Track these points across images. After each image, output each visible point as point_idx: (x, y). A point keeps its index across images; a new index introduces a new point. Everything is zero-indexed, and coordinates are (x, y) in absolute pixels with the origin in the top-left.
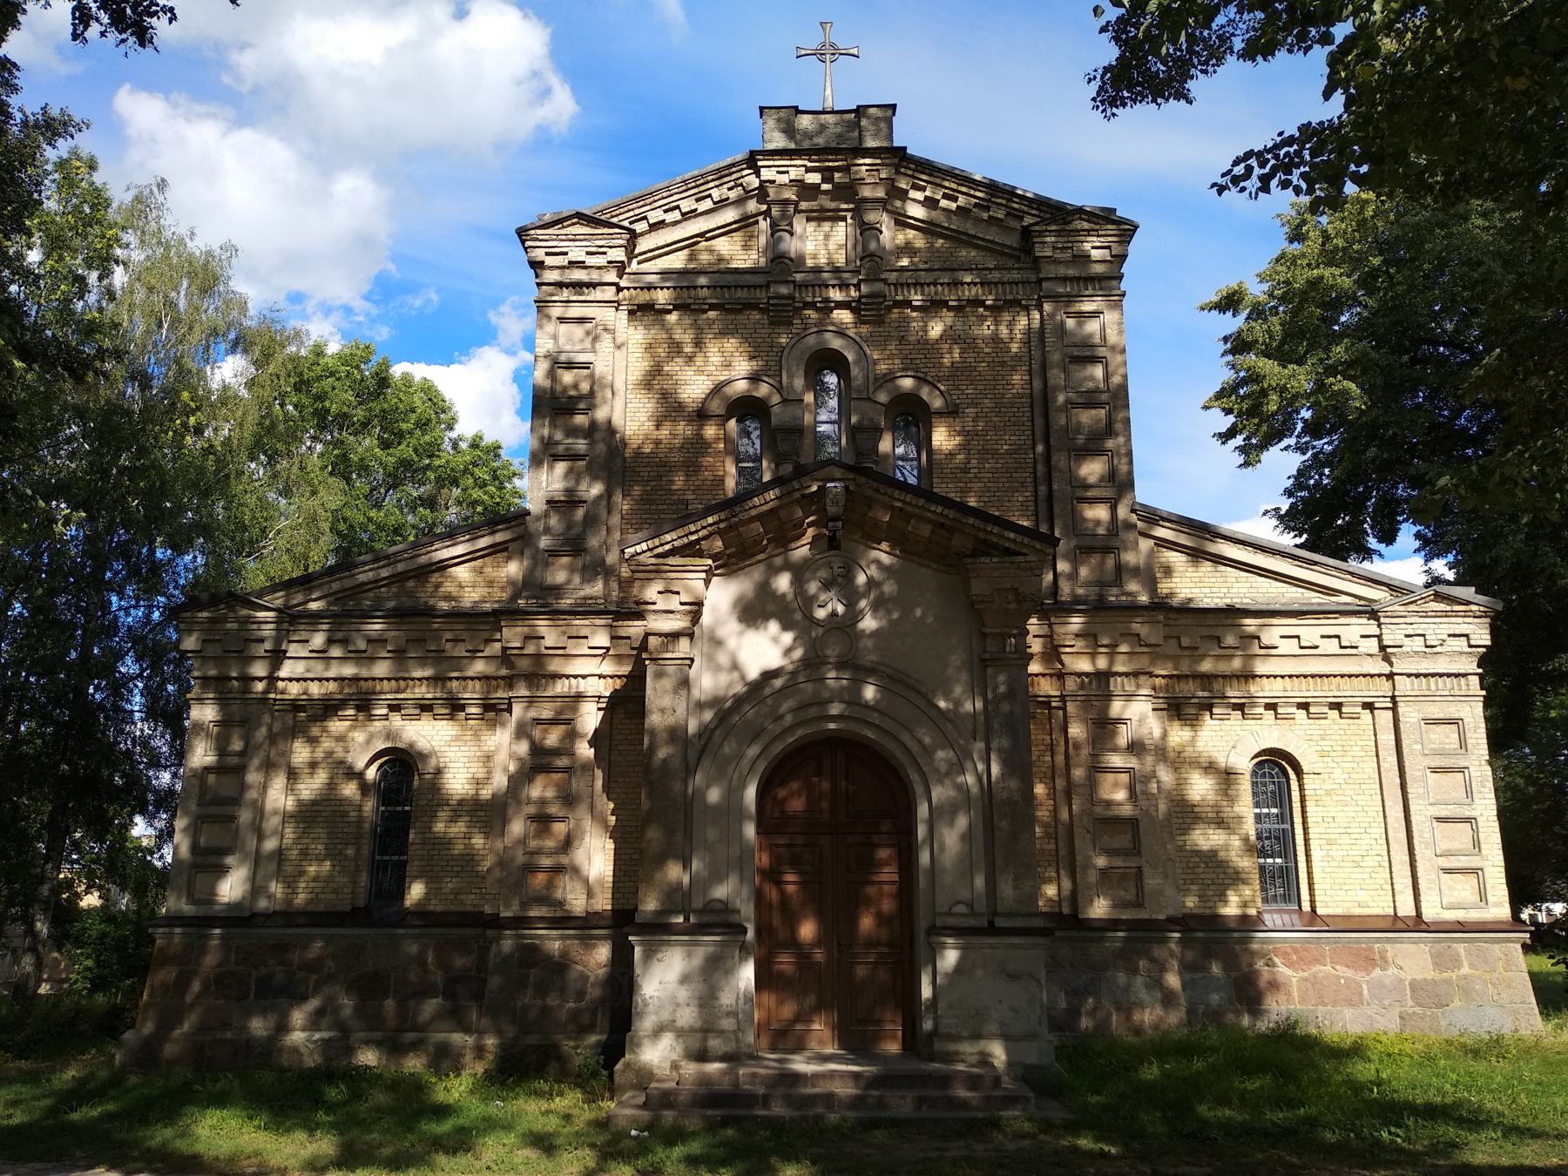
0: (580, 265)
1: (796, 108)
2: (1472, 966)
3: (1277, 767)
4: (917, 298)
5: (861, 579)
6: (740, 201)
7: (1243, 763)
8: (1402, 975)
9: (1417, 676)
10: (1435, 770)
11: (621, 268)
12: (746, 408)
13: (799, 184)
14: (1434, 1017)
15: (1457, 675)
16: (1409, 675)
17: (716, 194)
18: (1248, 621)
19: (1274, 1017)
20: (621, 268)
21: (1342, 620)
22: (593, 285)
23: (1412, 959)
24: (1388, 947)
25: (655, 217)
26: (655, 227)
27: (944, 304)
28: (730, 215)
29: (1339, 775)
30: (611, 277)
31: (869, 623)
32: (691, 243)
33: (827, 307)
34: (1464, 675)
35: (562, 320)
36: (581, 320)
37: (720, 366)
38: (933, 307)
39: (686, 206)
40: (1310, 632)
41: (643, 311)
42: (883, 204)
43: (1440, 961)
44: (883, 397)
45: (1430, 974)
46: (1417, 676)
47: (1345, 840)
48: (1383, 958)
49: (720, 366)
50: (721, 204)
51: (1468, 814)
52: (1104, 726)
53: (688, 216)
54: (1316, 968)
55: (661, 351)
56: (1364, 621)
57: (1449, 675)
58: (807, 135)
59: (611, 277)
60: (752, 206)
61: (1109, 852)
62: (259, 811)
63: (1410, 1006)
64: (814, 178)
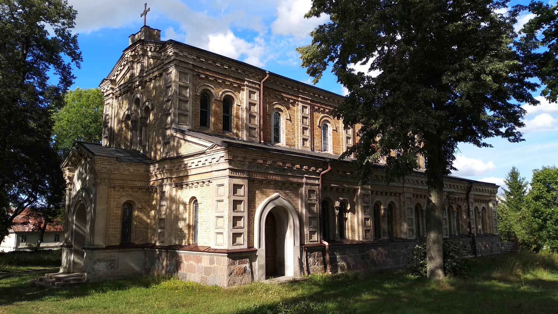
7: (187, 201)
11: (112, 89)
14: (207, 278)
17: (123, 64)
18: (185, 160)
19: (452, 279)
21: (201, 156)
22: (109, 94)
26: (117, 75)
28: (126, 68)
30: (111, 91)
31: (88, 178)
36: (108, 104)
43: (212, 262)
45: (208, 265)
46: (219, 170)
50: (124, 65)
53: (121, 70)
54: (190, 261)
59: (111, 91)
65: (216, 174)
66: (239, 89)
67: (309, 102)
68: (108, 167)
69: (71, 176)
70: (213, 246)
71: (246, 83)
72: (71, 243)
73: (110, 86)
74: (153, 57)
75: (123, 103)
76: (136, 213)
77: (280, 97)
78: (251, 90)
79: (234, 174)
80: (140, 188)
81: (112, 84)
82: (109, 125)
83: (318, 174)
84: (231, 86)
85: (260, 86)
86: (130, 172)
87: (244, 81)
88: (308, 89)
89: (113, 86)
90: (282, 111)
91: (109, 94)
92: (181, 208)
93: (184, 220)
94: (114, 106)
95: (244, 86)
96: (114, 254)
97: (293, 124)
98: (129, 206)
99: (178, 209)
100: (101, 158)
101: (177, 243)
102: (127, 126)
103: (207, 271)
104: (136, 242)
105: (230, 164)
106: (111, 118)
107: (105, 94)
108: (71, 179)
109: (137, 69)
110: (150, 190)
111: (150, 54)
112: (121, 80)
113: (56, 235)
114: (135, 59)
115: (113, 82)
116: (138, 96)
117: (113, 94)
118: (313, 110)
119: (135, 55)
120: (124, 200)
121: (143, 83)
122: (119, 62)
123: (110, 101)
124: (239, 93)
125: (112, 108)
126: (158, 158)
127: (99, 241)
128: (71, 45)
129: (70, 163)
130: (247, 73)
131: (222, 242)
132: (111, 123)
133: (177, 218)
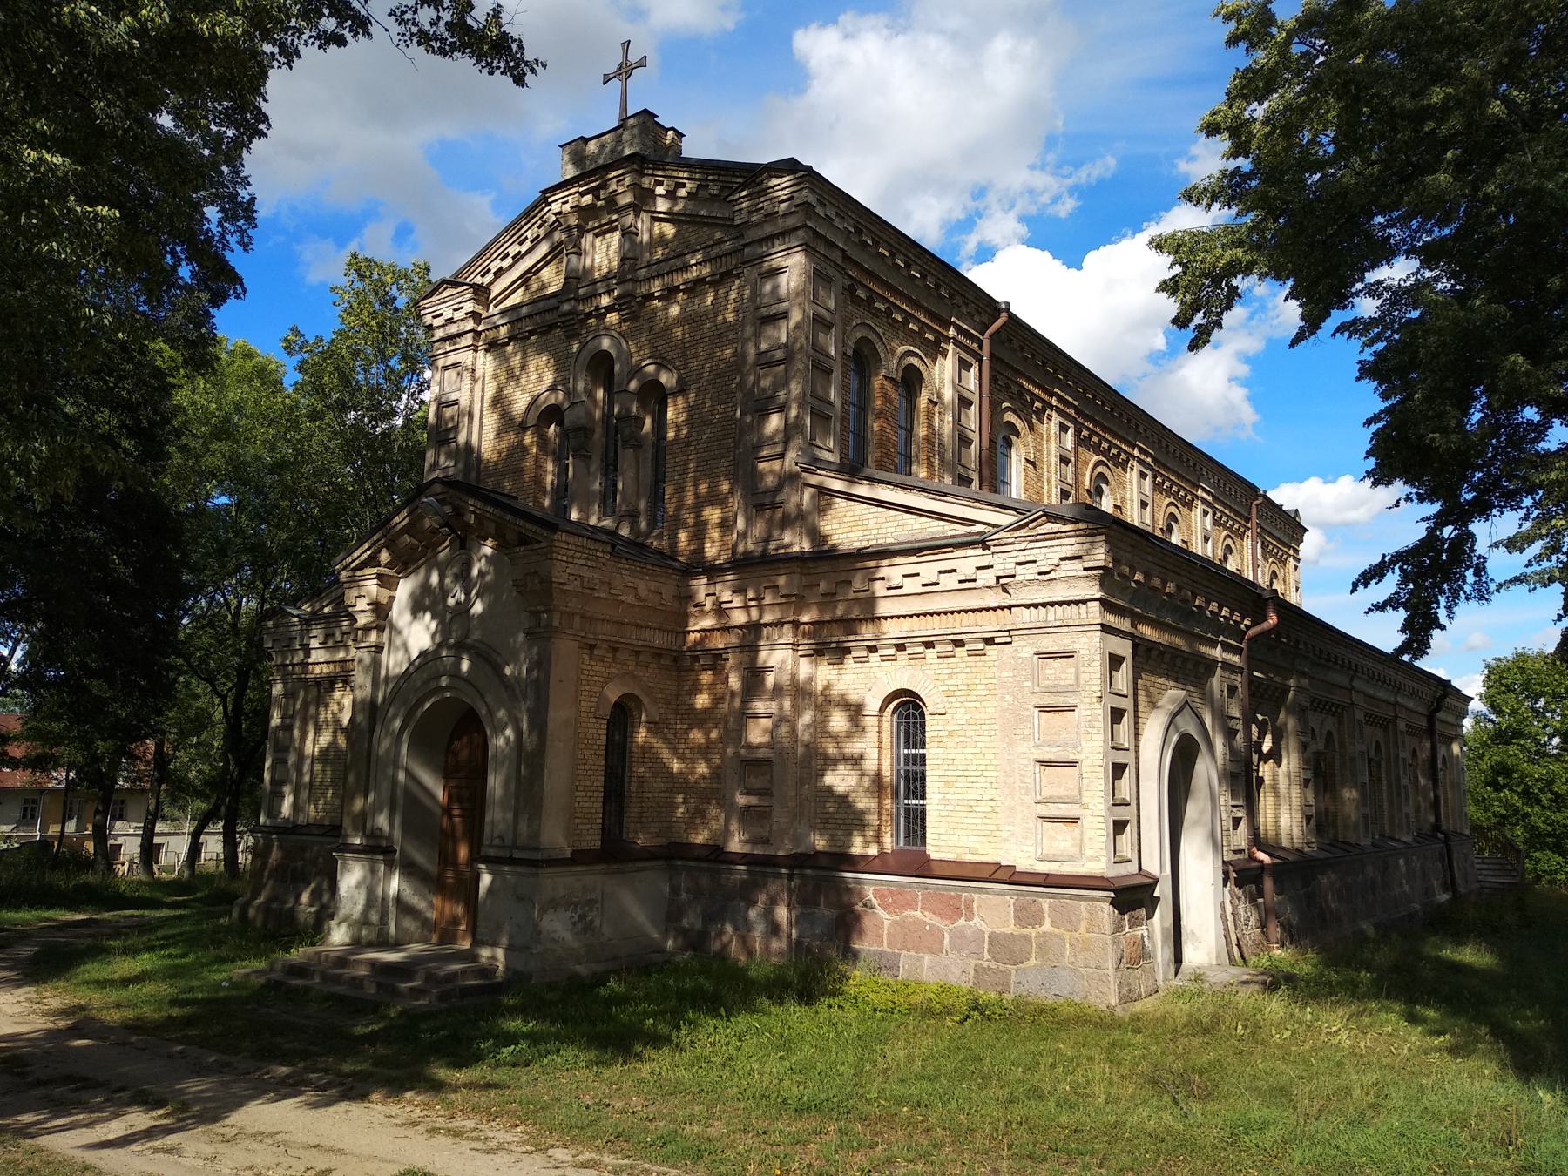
0: (450, 321)
1: (582, 138)
2: (1054, 924)
3: (908, 707)
4: (656, 287)
5: (475, 572)
6: (548, 235)
8: (984, 927)
9: (1036, 606)
10: (1044, 709)
11: (476, 316)
12: (552, 414)
13: (577, 208)
15: (1077, 603)
16: (1028, 606)
20: (476, 316)
21: (958, 553)
22: (461, 335)
23: (993, 911)
24: (976, 896)
25: (495, 266)
26: (499, 273)
27: (676, 289)
28: (544, 248)
29: (962, 716)
30: (470, 325)
31: (478, 608)
32: (525, 278)
33: (601, 314)
34: (1084, 602)
35: (445, 368)
36: (454, 366)
37: (537, 379)
38: (670, 293)
39: (513, 250)
40: (928, 569)
41: (493, 346)
42: (636, 208)
43: (1027, 916)
44: (633, 385)
45: (1011, 928)
46: (1036, 606)
47: (961, 783)
48: (969, 907)
49: (537, 379)
50: (536, 241)
51: (1071, 757)
52: (754, 676)
53: (518, 257)
55: (503, 379)
56: (979, 551)
57: (1068, 603)
58: (595, 157)
59: (470, 325)
60: (558, 236)
61: (749, 791)
62: (301, 757)
63: (986, 961)
64: (588, 199)
65: (1025, 617)
66: (935, 350)
67: (1072, 412)
68: (587, 574)
69: (384, 601)
70: (1025, 861)
71: (952, 332)
72: (390, 837)
73: (469, 306)
74: (671, 217)
75: (523, 366)
76: (642, 735)
77: (1015, 389)
78: (965, 356)
79: (1111, 620)
80: (658, 654)
81: (477, 301)
82: (462, 438)
83: (1240, 635)
84: (916, 338)
85: (980, 347)
86: (636, 596)
87: (947, 324)
88: (1075, 371)
89: (479, 309)
90: (1018, 435)
91: (461, 335)
92: (838, 721)
93: (856, 760)
94: (479, 373)
95: (947, 340)
96: (593, 880)
97: (1040, 479)
98: (621, 716)
99: (821, 726)
100: (572, 540)
101: (820, 843)
102: (542, 441)
103: (1006, 949)
104: (641, 841)
105: (1102, 586)
106: (471, 416)
107: (439, 334)
108: (381, 610)
109: (602, 254)
110: (684, 662)
111: (662, 206)
112: (510, 290)
113: (26, 801)
114: (590, 219)
115: (481, 293)
116: (606, 343)
117: (477, 334)
118: (1080, 441)
119: (592, 206)
120: (613, 694)
121: (632, 306)
122: (513, 229)
123: (466, 357)
124: (935, 361)
125: (474, 380)
126: (710, 550)
127: (554, 836)
128: (225, 168)
129: (384, 556)
130: (958, 300)
131: (1074, 851)
132: (470, 433)
133: (816, 760)
